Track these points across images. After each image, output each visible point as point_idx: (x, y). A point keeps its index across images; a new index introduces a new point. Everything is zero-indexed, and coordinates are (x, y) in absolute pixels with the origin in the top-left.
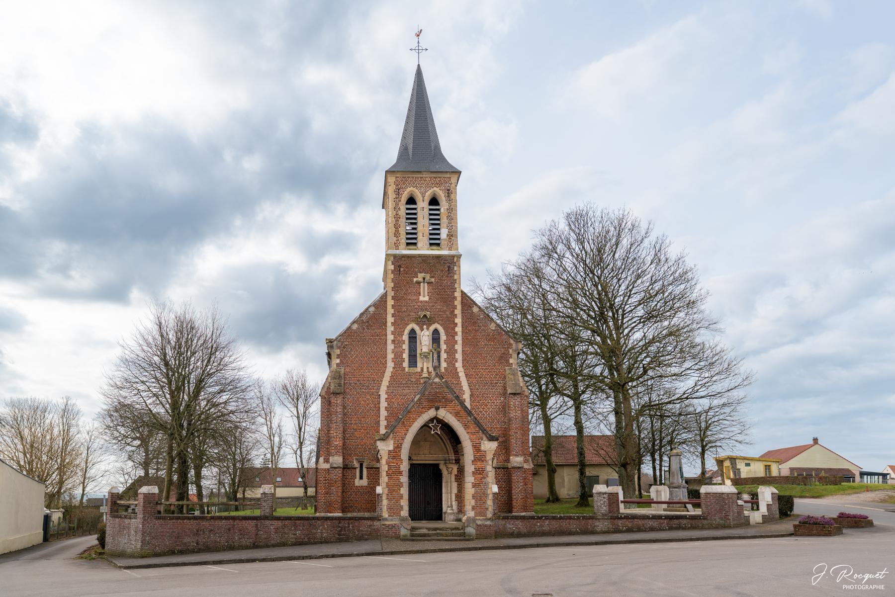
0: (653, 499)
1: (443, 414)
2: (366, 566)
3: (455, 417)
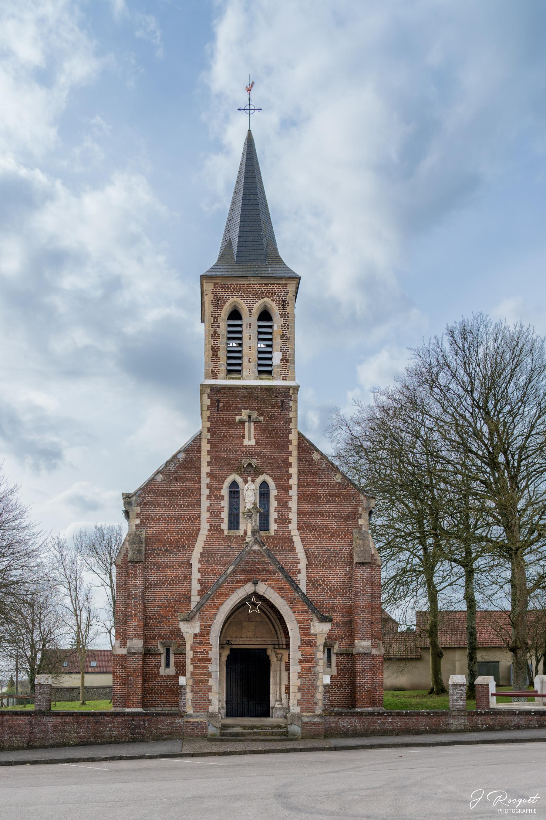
0: (536, 692)
1: (262, 589)
2: (149, 769)
3: (278, 593)
